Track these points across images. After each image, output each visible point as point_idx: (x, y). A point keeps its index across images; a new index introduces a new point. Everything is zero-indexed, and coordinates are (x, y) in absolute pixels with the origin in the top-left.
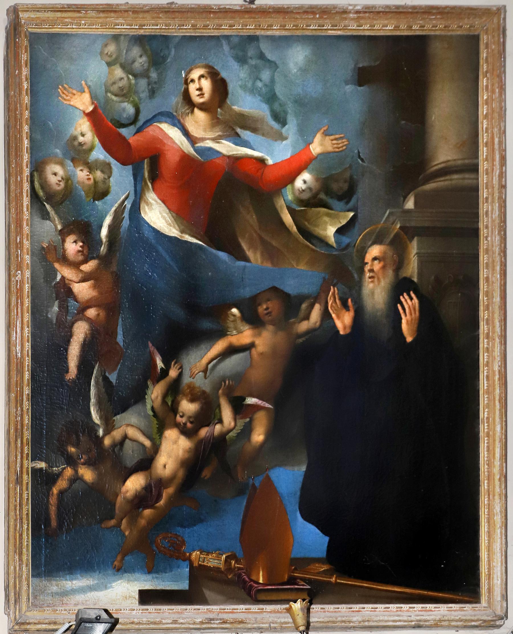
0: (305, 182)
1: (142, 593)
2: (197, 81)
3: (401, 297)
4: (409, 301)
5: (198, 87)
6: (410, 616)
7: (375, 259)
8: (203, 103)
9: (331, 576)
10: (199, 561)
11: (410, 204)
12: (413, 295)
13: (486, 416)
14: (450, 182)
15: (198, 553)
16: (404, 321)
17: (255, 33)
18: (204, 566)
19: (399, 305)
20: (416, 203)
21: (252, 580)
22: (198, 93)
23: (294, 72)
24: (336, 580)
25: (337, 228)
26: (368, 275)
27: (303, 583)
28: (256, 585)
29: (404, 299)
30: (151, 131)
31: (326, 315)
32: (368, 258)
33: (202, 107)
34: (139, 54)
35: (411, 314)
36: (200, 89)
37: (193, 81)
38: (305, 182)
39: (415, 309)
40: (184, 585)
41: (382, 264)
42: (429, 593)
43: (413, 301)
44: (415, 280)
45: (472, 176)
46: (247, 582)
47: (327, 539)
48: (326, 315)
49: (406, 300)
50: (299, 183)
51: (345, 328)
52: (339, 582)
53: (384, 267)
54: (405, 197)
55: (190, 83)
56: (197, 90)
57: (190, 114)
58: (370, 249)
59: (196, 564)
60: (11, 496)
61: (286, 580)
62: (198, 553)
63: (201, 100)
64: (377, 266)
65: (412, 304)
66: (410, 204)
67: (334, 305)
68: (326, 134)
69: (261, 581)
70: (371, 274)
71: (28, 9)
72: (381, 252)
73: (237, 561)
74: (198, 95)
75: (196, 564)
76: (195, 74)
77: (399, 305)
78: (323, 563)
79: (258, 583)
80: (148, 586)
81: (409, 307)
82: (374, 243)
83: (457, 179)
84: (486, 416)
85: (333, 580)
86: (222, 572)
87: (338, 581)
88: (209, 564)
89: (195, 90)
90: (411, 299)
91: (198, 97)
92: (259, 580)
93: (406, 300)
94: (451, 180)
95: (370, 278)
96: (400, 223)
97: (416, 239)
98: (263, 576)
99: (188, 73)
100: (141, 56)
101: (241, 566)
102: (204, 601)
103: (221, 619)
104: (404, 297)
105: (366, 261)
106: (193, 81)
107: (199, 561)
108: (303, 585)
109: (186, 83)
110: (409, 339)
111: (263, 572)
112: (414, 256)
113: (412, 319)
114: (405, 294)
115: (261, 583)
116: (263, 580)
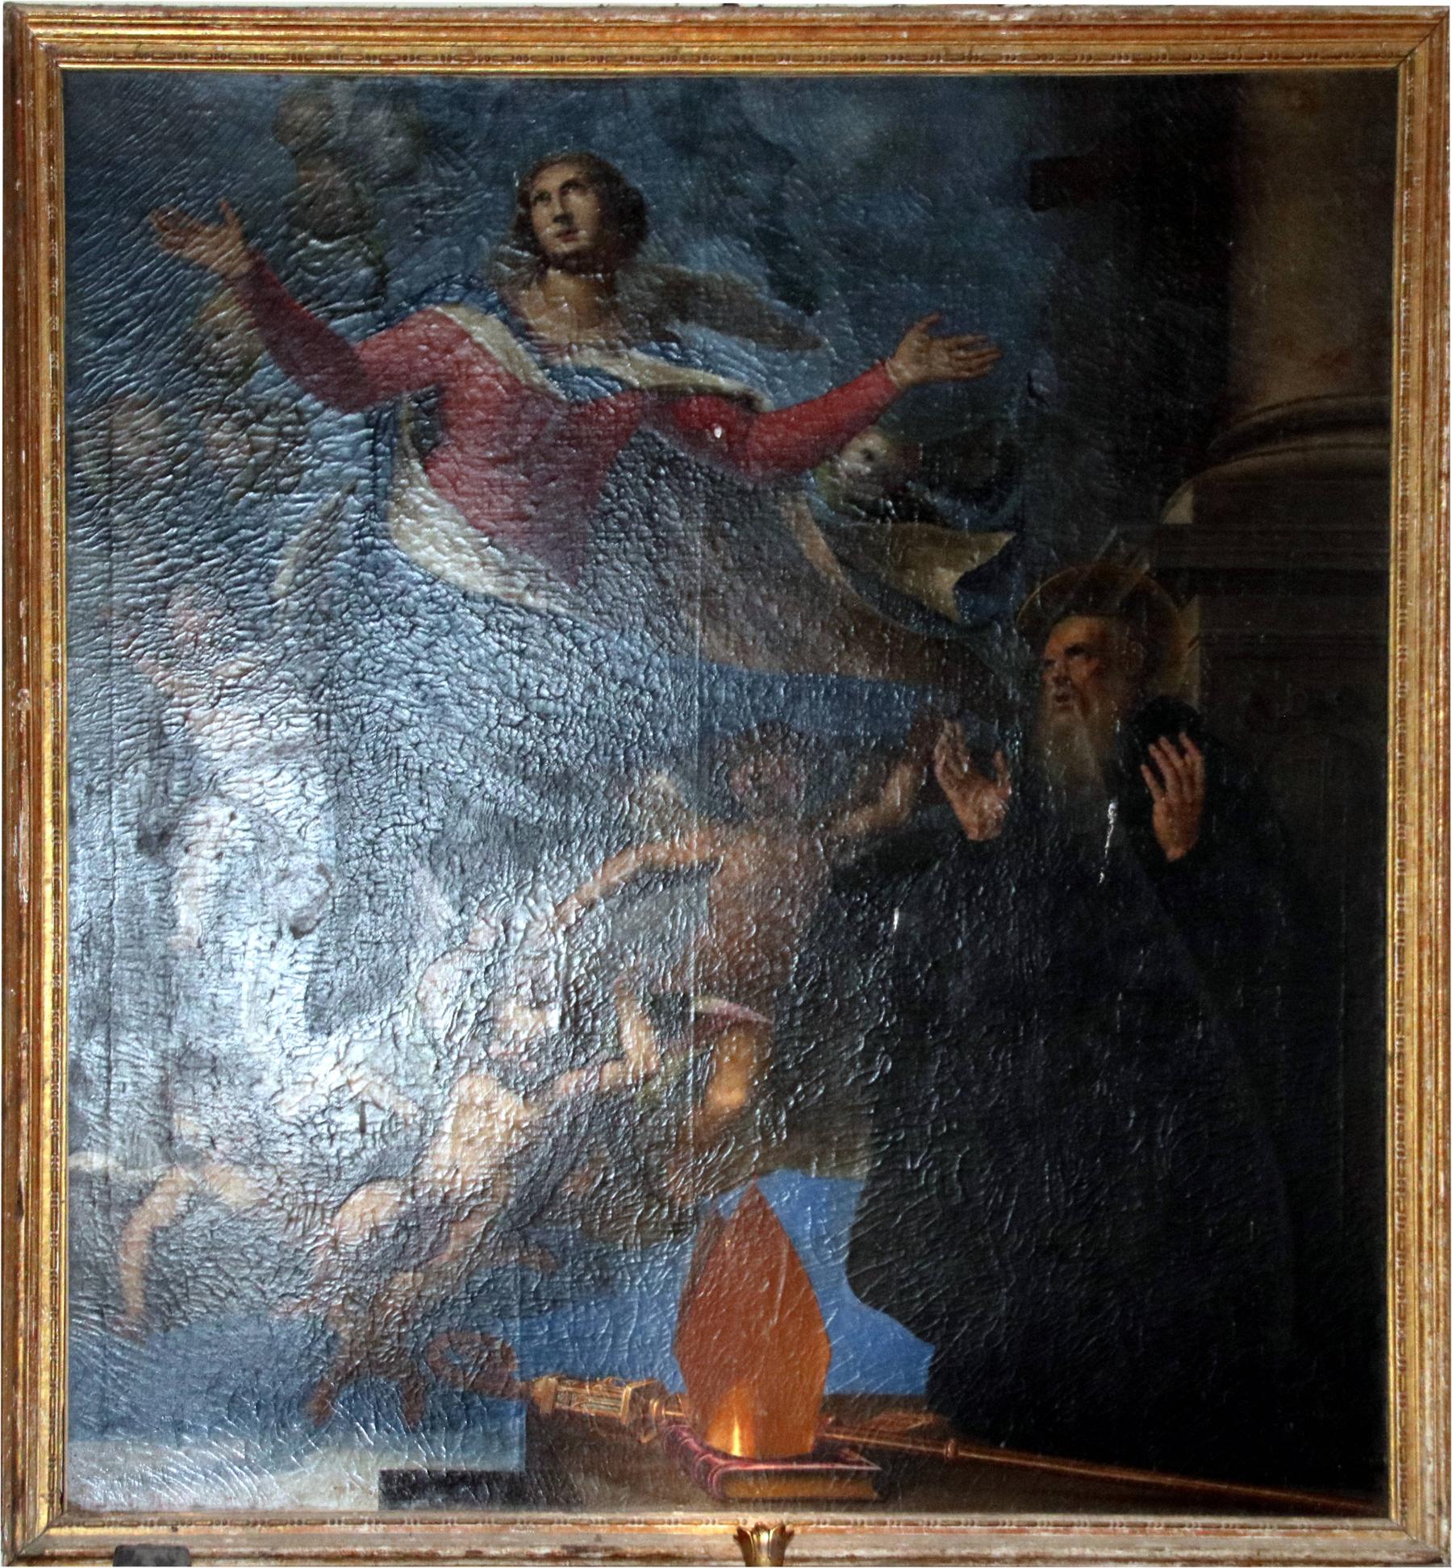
0: (869, 456)
1: (386, 1477)
2: (555, 197)
3: (1152, 748)
4: (1174, 756)
5: (558, 211)
6: (1161, 1550)
7: (1073, 651)
8: (576, 254)
9: (943, 1440)
10: (556, 1400)
11: (1181, 511)
12: (1186, 743)
13: (1397, 1050)
14: (1300, 455)
15: (553, 1380)
16: (1159, 808)
17: (1409, 184)
18: (572, 1414)
19: (1143, 767)
20: (1197, 508)
21: (709, 1450)
22: (557, 228)
23: (843, 173)
24: (956, 1453)
25: (960, 574)
26: (1053, 691)
27: (857, 1457)
28: (722, 1462)
29: (1163, 752)
30: (421, 327)
31: (929, 794)
32: (1055, 647)
33: (574, 265)
34: (387, 127)
35: (1180, 791)
36: (565, 218)
37: (544, 197)
38: (869, 456)
39: (1191, 777)
40: (513, 1461)
41: (1094, 663)
42: (1235, 1488)
43: (1187, 758)
44: (1194, 701)
45: (1370, 439)
46: (696, 1452)
47: (927, 1355)
48: (929, 794)
49: (1166, 756)
50: (851, 461)
51: (982, 826)
52: (963, 1458)
53: (1098, 673)
54: (1168, 492)
55: (535, 204)
56: (556, 220)
57: (534, 284)
58: (1060, 626)
59: (546, 1409)
60: (1426, 1070)
61: (809, 1450)
62: (553, 1380)
63: (566, 248)
64: (1081, 670)
65: (1185, 764)
66: (1181, 511)
67: (952, 765)
68: (935, 330)
69: (736, 1451)
70: (1062, 690)
71: (52, 17)
72: (1091, 635)
73: (667, 1402)
74: (559, 235)
75: (546, 1409)
76: (552, 180)
77: (1143, 767)
78: (917, 1409)
79: (726, 1456)
80: (401, 1462)
81: (1176, 772)
82: (1080, 609)
83: (1321, 447)
84: (1397, 1050)
85: (948, 1450)
86: (621, 1429)
87: (961, 1454)
88: (585, 1410)
89: (550, 220)
90: (1182, 752)
91: (557, 241)
92: (731, 1449)
93: (1166, 756)
94: (1304, 450)
95: (1059, 698)
96: (1151, 562)
97: (1196, 599)
98: (742, 1438)
99: (535, 173)
100: (391, 133)
101: (678, 1414)
102: (566, 1500)
103: (606, 1549)
104: (1159, 748)
105: (1048, 654)
106: (544, 197)
107: (556, 1400)
108: (860, 1463)
109: (525, 201)
110: (1174, 853)
111: (742, 1428)
112: (1192, 643)
113: (1183, 803)
114: (1163, 740)
115: (735, 1458)
116: (743, 1449)
